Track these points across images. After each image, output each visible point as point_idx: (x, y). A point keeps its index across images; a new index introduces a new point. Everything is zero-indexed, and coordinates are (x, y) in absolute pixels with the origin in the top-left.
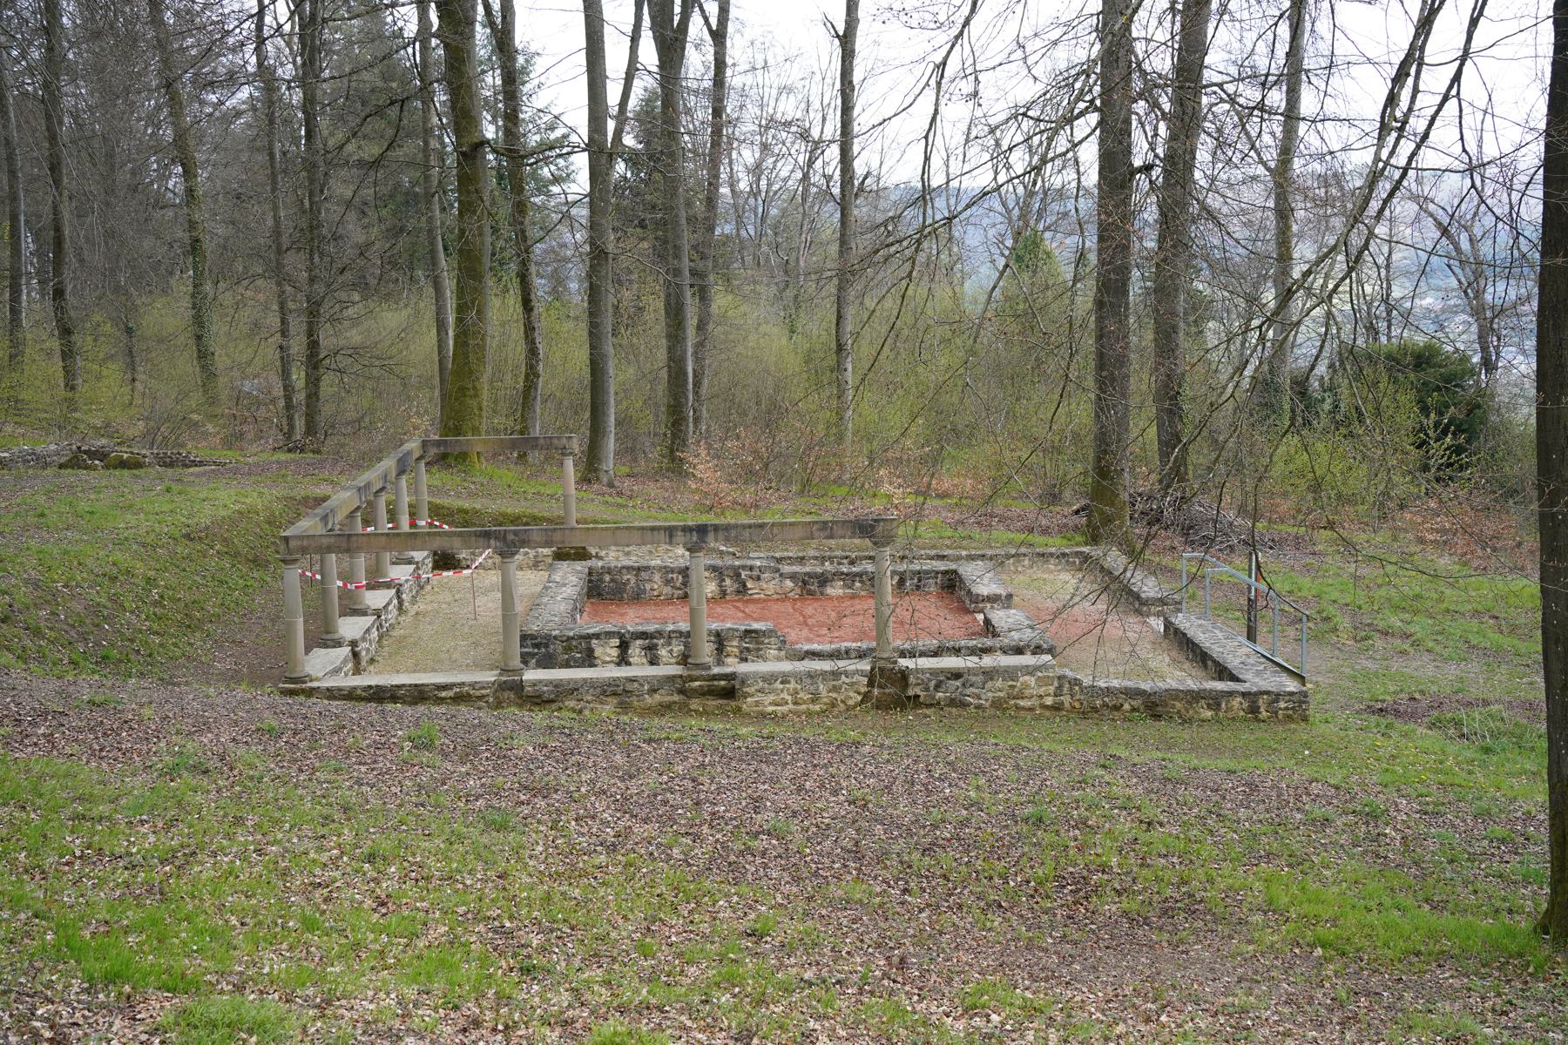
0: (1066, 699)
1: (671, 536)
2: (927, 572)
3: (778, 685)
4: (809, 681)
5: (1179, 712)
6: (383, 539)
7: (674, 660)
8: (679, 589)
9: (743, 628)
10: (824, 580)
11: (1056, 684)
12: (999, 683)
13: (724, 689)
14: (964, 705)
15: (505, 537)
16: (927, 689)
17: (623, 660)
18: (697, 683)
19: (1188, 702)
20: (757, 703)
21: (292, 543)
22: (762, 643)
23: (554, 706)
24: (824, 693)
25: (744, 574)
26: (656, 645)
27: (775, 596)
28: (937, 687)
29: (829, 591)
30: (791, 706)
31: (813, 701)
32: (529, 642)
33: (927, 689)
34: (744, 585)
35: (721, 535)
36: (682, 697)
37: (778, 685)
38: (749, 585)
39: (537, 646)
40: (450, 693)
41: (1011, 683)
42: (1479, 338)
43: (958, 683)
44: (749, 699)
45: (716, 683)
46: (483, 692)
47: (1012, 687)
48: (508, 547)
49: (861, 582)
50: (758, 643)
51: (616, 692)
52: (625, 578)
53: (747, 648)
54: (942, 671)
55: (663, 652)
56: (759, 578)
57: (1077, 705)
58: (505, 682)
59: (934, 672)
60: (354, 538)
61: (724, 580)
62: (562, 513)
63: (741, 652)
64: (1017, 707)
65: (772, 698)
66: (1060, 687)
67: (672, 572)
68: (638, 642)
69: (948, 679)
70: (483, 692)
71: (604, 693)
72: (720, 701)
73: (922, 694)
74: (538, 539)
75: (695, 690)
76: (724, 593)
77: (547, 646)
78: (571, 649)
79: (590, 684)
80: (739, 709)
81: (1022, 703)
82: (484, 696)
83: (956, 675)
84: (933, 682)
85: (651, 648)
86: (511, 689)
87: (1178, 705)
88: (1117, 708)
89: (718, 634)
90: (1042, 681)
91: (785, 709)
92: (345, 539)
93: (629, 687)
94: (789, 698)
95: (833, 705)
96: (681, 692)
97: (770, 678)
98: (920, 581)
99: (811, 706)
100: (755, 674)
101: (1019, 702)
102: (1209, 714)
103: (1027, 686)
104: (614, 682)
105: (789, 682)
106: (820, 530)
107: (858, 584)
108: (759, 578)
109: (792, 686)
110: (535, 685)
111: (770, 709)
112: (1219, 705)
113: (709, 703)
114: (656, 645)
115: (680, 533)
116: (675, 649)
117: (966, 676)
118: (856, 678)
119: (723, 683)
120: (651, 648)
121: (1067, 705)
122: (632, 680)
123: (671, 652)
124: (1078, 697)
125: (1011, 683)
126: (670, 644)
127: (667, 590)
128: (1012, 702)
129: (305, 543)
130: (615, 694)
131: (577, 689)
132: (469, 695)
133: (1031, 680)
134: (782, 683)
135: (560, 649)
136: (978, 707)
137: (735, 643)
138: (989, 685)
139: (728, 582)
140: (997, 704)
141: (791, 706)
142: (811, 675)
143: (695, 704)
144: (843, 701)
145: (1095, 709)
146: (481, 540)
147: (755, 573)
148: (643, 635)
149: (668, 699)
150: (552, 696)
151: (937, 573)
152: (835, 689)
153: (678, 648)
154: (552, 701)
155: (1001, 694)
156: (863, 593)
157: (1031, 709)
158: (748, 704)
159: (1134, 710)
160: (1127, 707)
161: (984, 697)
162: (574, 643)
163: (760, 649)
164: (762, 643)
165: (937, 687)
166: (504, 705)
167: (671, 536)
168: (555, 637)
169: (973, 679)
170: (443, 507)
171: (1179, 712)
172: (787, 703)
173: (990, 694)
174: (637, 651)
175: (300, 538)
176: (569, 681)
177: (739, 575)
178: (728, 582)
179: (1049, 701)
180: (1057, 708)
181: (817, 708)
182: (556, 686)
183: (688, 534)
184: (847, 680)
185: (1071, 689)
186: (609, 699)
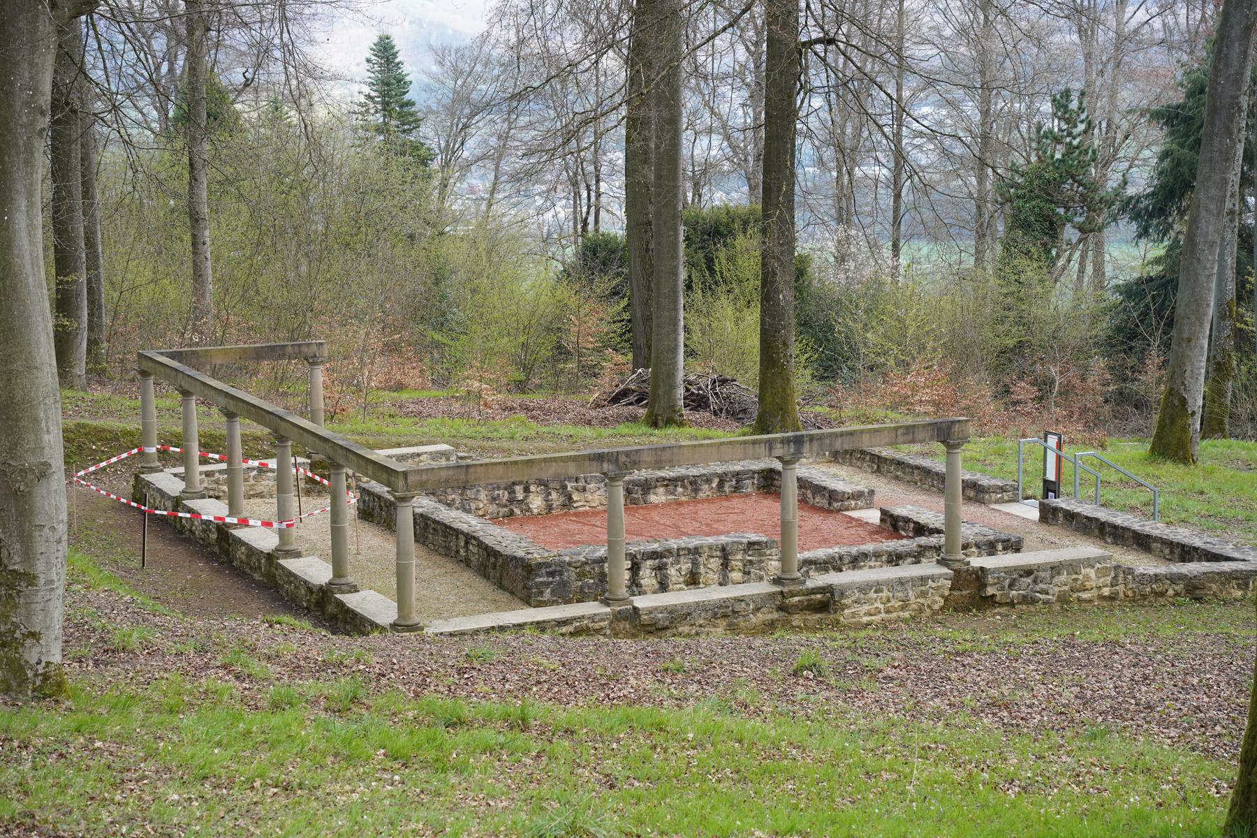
0: (1121, 588)
1: (770, 449)
2: (745, 473)
3: (872, 595)
4: (899, 588)
5: (1214, 594)
6: (501, 468)
7: (682, 579)
8: (506, 506)
9: (745, 541)
10: (647, 487)
11: (1112, 574)
12: (1063, 577)
13: (821, 602)
14: (1034, 601)
15: (617, 459)
16: (1003, 588)
17: (693, 580)
18: (797, 599)
19: (1222, 583)
20: (854, 615)
21: (411, 479)
22: (765, 555)
23: (668, 633)
24: (913, 600)
25: (570, 485)
26: (666, 564)
27: (600, 508)
28: (1011, 586)
29: (653, 498)
30: (883, 615)
31: (903, 608)
32: (544, 571)
33: (1003, 588)
34: (570, 498)
35: (816, 444)
36: (782, 614)
37: (872, 595)
38: (575, 497)
39: (551, 574)
40: (571, 628)
41: (1074, 576)
42: (38, 16)
43: (1029, 580)
44: (846, 611)
45: (813, 597)
46: (602, 624)
47: (1076, 580)
48: (620, 469)
49: (683, 486)
50: (760, 555)
51: (726, 613)
52: (450, 498)
53: (750, 561)
54: (1016, 569)
55: (672, 571)
56: (584, 490)
57: (1130, 594)
58: (619, 612)
59: (1008, 570)
60: (472, 470)
61: (550, 494)
62: (179, 430)
63: (745, 565)
64: (1079, 600)
65: (866, 607)
66: (1116, 577)
67: (499, 488)
68: (649, 562)
69: (1021, 576)
70: (602, 624)
71: (715, 616)
72: (819, 616)
73: (998, 593)
74: (648, 459)
75: (795, 606)
76: (550, 508)
77: (561, 573)
78: (585, 575)
79: (702, 607)
80: (838, 622)
81: (1085, 595)
82: (602, 628)
83: (1028, 572)
84: (1008, 581)
85: (661, 568)
86: (626, 619)
87: (1214, 586)
88: (1162, 594)
89: (723, 549)
90: (1101, 573)
91: (877, 618)
92: (463, 470)
93: (738, 607)
94: (882, 607)
95: (921, 611)
96: (782, 608)
97: (864, 588)
98: (737, 482)
99: (901, 614)
100: (850, 586)
101: (1080, 594)
102: (1239, 594)
103: (1087, 578)
104: (723, 604)
105: (882, 591)
106: (904, 434)
107: (680, 490)
108: (584, 490)
109: (884, 594)
110: (651, 612)
111: (865, 619)
112: (1247, 585)
113: (809, 617)
114: (666, 564)
115: (779, 446)
116: (684, 567)
117: (1036, 573)
118: (942, 582)
119: (819, 596)
120: (661, 568)
121: (1121, 595)
122: (739, 600)
123: (679, 570)
124: (1130, 586)
125: (1074, 576)
126: (678, 562)
127: (492, 508)
128: (1075, 595)
129: (424, 477)
130: (725, 616)
131: (689, 614)
132: (588, 628)
133: (1092, 573)
134: (876, 592)
135: (574, 576)
136: (1046, 602)
137: (739, 557)
138: (1056, 580)
139: (554, 495)
140: (1063, 599)
141: (883, 615)
142: (901, 582)
143: (797, 620)
144: (929, 606)
145: (1144, 597)
146: (595, 463)
147: (581, 484)
148: (654, 555)
149: (769, 617)
150: (667, 623)
151: (754, 472)
152: (923, 594)
153: (686, 566)
154: (666, 628)
155: (1066, 588)
156: (683, 499)
157: (1090, 601)
158: (845, 616)
159: (1177, 594)
160: (1171, 592)
161: (1051, 592)
162: (587, 568)
163: (761, 561)
164: (765, 555)
165: (1011, 586)
166: (621, 636)
167: (770, 449)
168: (569, 564)
169: (1042, 574)
170: (104, 430)
171: (1214, 594)
172: (880, 612)
173: (1057, 589)
174: (648, 571)
175: (420, 472)
176: (683, 606)
177: (565, 487)
178: (554, 495)
179: (1106, 591)
180: (1112, 598)
181: (906, 615)
182: (671, 612)
183: (786, 446)
184: (934, 585)
185: (1125, 579)
186: (718, 621)
